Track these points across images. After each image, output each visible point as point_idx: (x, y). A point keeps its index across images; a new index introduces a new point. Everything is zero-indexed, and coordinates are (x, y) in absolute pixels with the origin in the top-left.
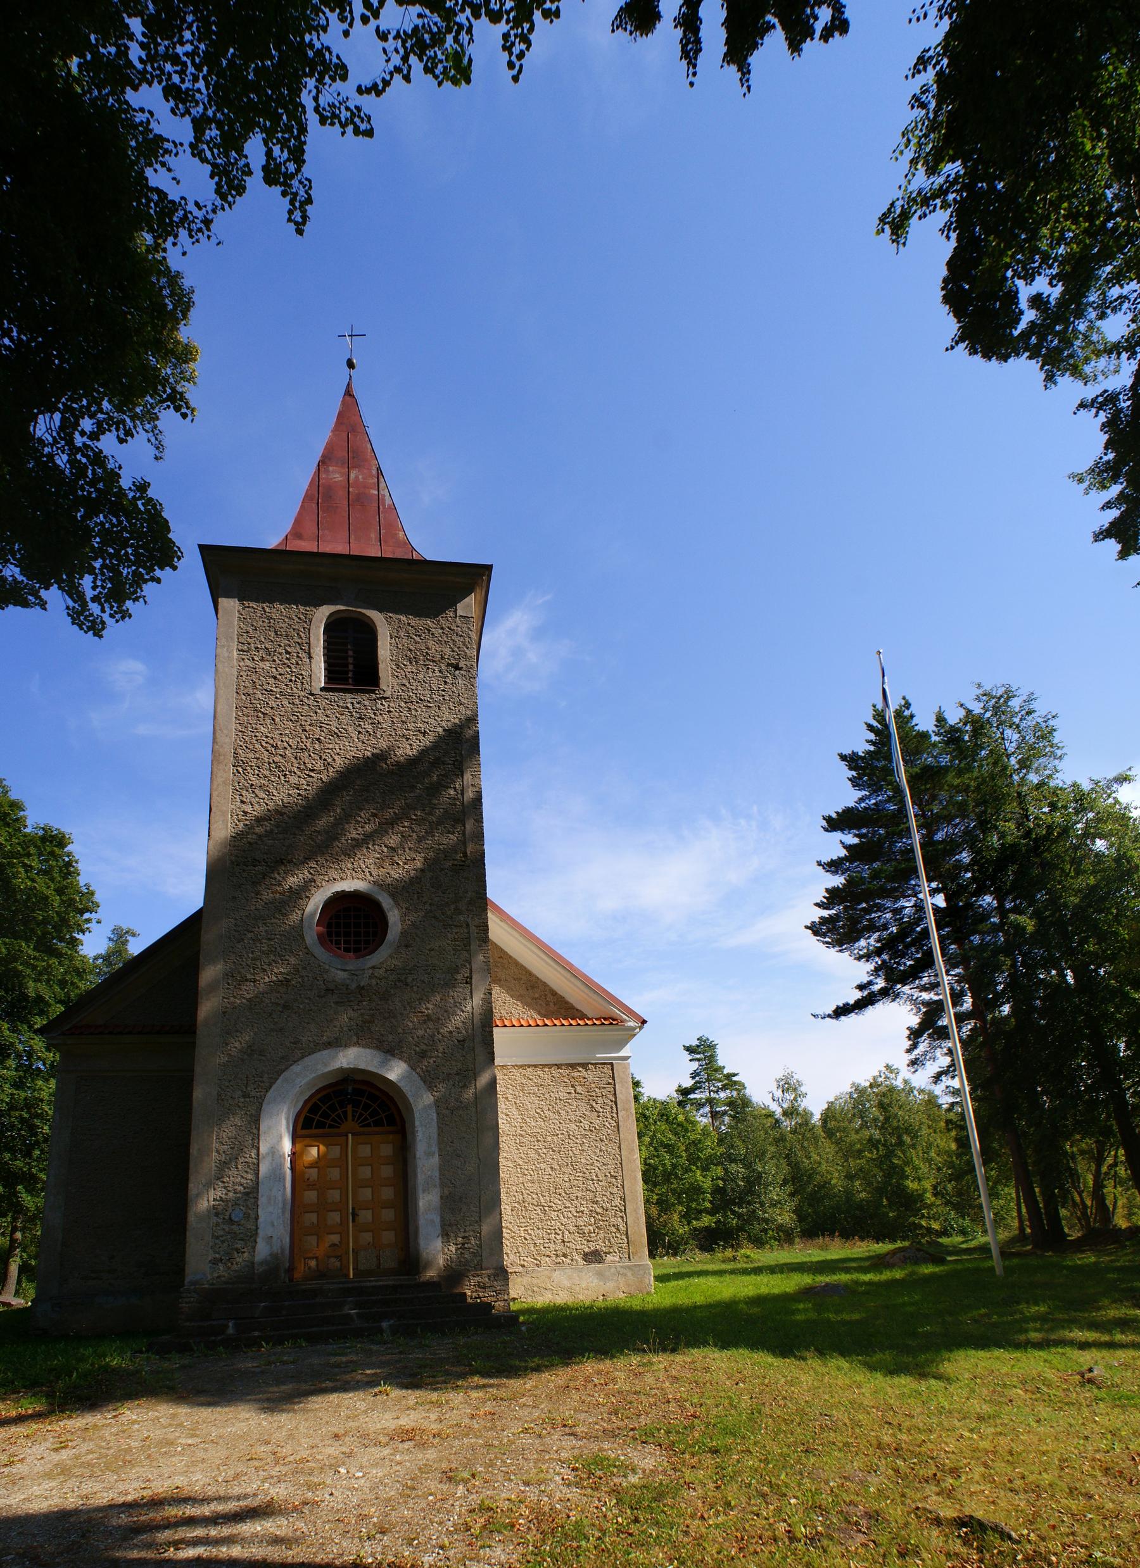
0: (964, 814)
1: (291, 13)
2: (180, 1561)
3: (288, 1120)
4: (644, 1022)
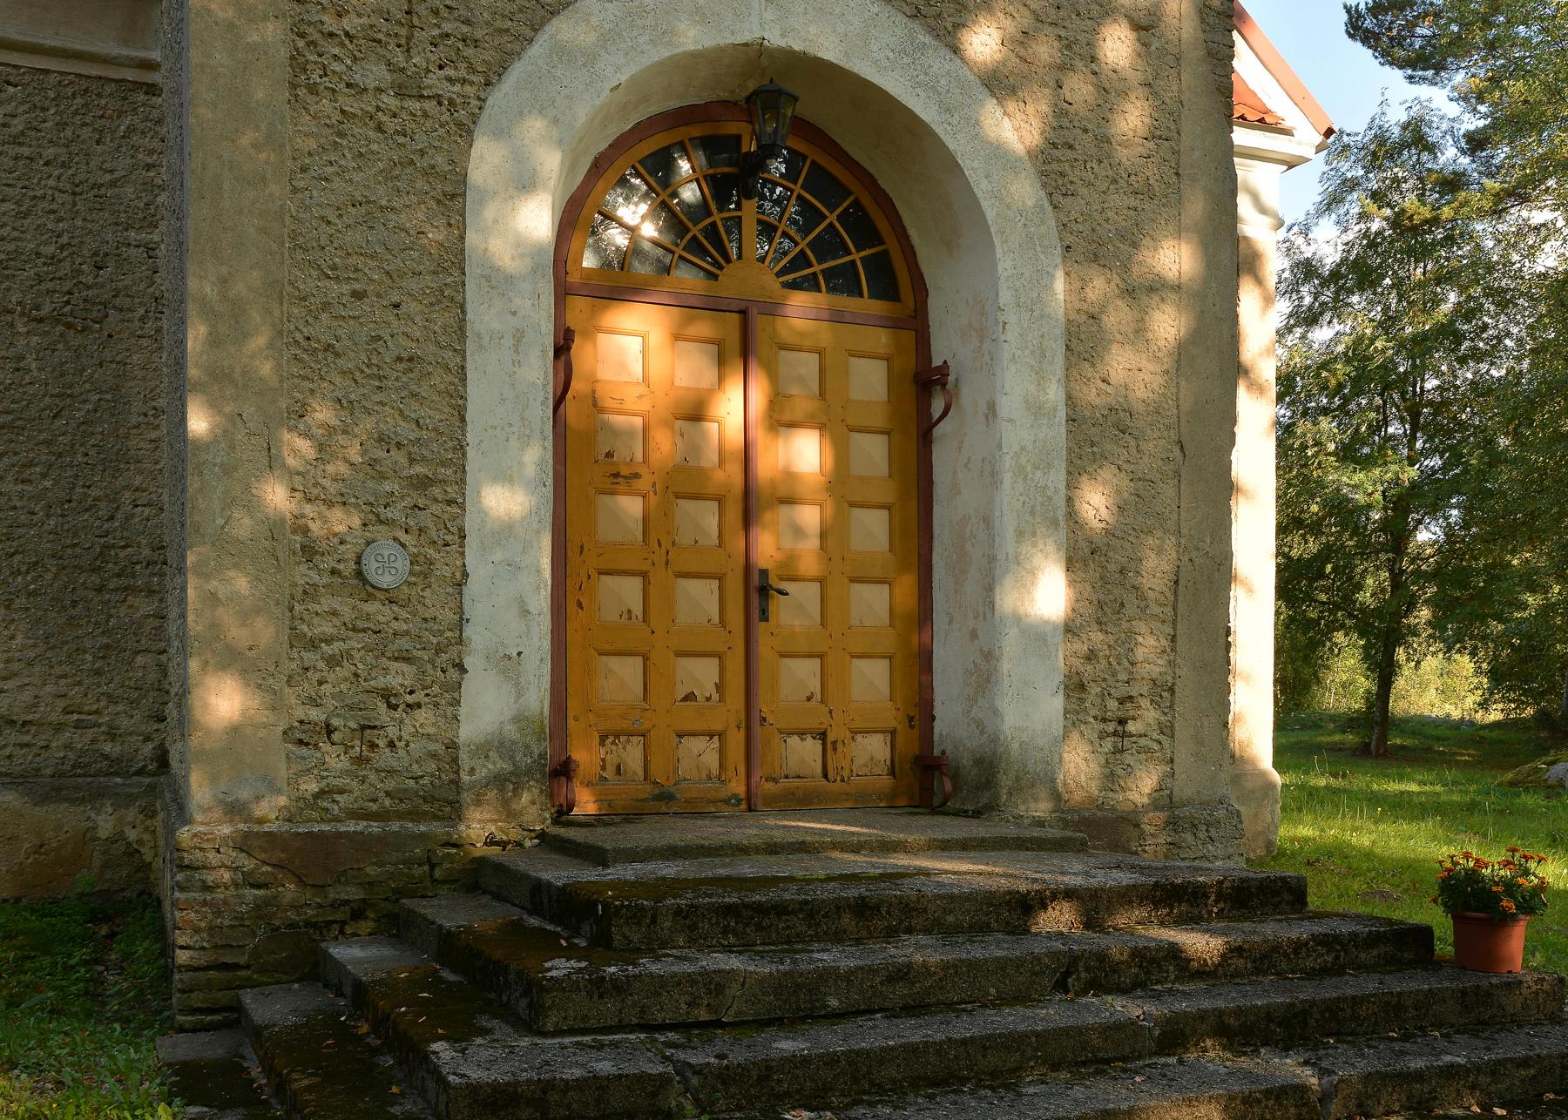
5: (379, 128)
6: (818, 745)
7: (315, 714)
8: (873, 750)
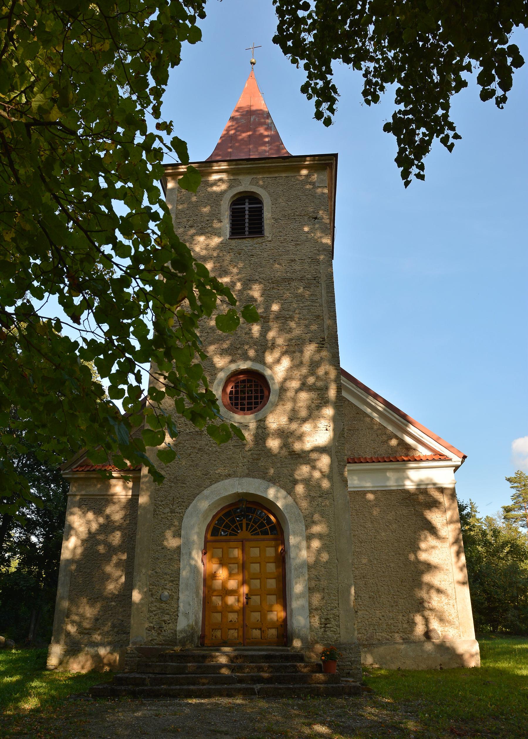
0: (520, 483)
2: (518, 676)
4: (465, 457)
5: (168, 519)
6: (260, 631)
7: (152, 625)
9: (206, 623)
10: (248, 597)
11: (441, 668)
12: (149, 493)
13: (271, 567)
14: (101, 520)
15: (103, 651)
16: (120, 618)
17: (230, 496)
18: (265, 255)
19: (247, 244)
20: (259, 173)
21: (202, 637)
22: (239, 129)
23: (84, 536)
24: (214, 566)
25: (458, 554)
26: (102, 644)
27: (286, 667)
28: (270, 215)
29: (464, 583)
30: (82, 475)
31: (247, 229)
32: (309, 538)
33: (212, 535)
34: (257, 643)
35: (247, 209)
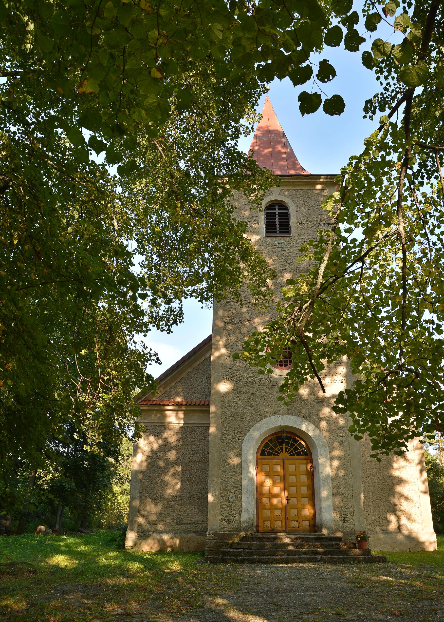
1: (429, 143)
3: (254, 450)
7: (223, 517)
8: (306, 523)
9: (259, 516)
10: (288, 499)
11: (410, 551)
12: (215, 425)
13: (304, 478)
14: (160, 442)
15: (166, 537)
16: (178, 513)
17: (275, 428)
18: (293, 250)
19: (279, 241)
20: (286, 186)
21: (257, 526)
22: (262, 145)
23: (148, 453)
24: (262, 477)
25: (421, 471)
26: (166, 532)
27: (333, 545)
28: (295, 220)
29: (425, 493)
30: (145, 408)
31: (278, 229)
32: (332, 459)
33: (261, 455)
34: (295, 531)
35: (277, 213)
